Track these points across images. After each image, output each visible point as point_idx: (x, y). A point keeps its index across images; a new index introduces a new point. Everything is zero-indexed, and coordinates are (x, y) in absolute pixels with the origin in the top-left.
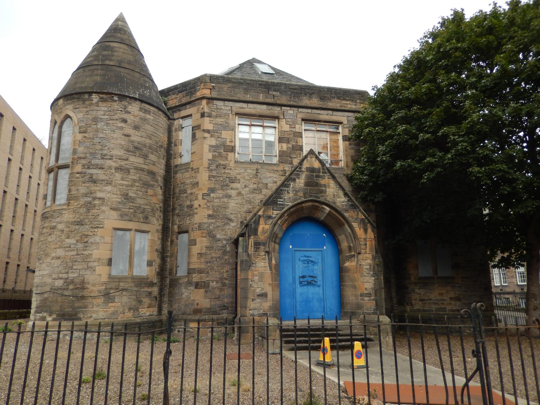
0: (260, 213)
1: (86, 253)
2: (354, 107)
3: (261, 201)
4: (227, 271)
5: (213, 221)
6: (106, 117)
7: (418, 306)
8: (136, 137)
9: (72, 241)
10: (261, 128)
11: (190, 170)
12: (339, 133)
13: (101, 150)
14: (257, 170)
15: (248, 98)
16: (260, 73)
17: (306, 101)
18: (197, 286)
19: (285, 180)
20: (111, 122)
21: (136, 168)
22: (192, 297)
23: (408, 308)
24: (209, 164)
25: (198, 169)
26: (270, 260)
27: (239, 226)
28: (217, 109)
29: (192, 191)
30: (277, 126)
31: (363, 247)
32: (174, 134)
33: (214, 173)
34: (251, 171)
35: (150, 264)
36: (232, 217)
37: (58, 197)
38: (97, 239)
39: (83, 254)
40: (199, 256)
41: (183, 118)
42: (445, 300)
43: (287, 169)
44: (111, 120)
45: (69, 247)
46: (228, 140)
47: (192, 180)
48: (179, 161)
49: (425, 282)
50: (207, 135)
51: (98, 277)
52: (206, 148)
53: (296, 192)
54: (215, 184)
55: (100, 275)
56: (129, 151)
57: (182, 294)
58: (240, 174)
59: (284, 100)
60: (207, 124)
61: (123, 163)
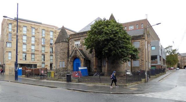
8: (61, 48)
15: (76, 37)
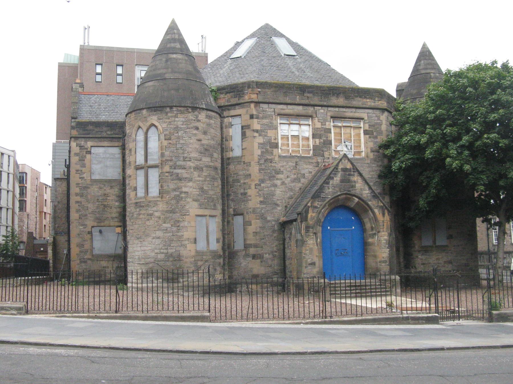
0: (309, 204)
1: (179, 234)
2: (373, 104)
3: (300, 189)
4: (276, 246)
5: (264, 206)
6: (184, 126)
7: (420, 268)
9: (169, 225)
10: (298, 126)
11: (242, 163)
12: (361, 127)
13: (183, 153)
14: (296, 162)
15: (288, 100)
16: (283, 55)
17: (334, 101)
18: (254, 257)
19: (327, 179)
20: (188, 130)
21: (207, 166)
22: (248, 266)
23: (413, 271)
24: (259, 159)
25: (250, 163)
26: (317, 238)
27: (284, 209)
28: (263, 111)
29: (245, 181)
30: (311, 123)
31: (382, 227)
32: (224, 130)
33: (263, 167)
34: (292, 164)
35: (218, 241)
36: (278, 202)
37: (150, 190)
38: (186, 224)
39: (177, 235)
40: (255, 234)
41: (232, 116)
42: (441, 263)
43: (319, 161)
44: (188, 128)
45: (166, 230)
46: (273, 138)
47: (244, 172)
48: (231, 155)
49: (426, 250)
50: (256, 134)
51: (188, 251)
52: (256, 145)
53: (334, 187)
54: (264, 176)
55: (190, 250)
56: (201, 153)
57: (240, 264)
58: (283, 166)
59: (316, 100)
60: (256, 125)
61: (198, 163)
